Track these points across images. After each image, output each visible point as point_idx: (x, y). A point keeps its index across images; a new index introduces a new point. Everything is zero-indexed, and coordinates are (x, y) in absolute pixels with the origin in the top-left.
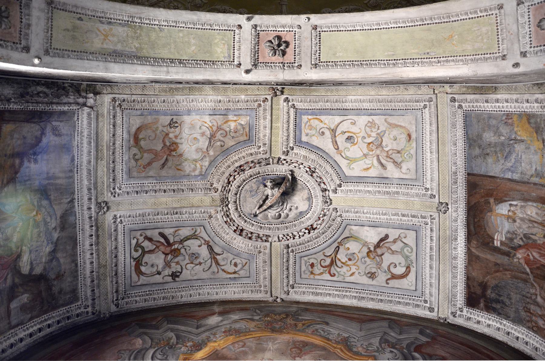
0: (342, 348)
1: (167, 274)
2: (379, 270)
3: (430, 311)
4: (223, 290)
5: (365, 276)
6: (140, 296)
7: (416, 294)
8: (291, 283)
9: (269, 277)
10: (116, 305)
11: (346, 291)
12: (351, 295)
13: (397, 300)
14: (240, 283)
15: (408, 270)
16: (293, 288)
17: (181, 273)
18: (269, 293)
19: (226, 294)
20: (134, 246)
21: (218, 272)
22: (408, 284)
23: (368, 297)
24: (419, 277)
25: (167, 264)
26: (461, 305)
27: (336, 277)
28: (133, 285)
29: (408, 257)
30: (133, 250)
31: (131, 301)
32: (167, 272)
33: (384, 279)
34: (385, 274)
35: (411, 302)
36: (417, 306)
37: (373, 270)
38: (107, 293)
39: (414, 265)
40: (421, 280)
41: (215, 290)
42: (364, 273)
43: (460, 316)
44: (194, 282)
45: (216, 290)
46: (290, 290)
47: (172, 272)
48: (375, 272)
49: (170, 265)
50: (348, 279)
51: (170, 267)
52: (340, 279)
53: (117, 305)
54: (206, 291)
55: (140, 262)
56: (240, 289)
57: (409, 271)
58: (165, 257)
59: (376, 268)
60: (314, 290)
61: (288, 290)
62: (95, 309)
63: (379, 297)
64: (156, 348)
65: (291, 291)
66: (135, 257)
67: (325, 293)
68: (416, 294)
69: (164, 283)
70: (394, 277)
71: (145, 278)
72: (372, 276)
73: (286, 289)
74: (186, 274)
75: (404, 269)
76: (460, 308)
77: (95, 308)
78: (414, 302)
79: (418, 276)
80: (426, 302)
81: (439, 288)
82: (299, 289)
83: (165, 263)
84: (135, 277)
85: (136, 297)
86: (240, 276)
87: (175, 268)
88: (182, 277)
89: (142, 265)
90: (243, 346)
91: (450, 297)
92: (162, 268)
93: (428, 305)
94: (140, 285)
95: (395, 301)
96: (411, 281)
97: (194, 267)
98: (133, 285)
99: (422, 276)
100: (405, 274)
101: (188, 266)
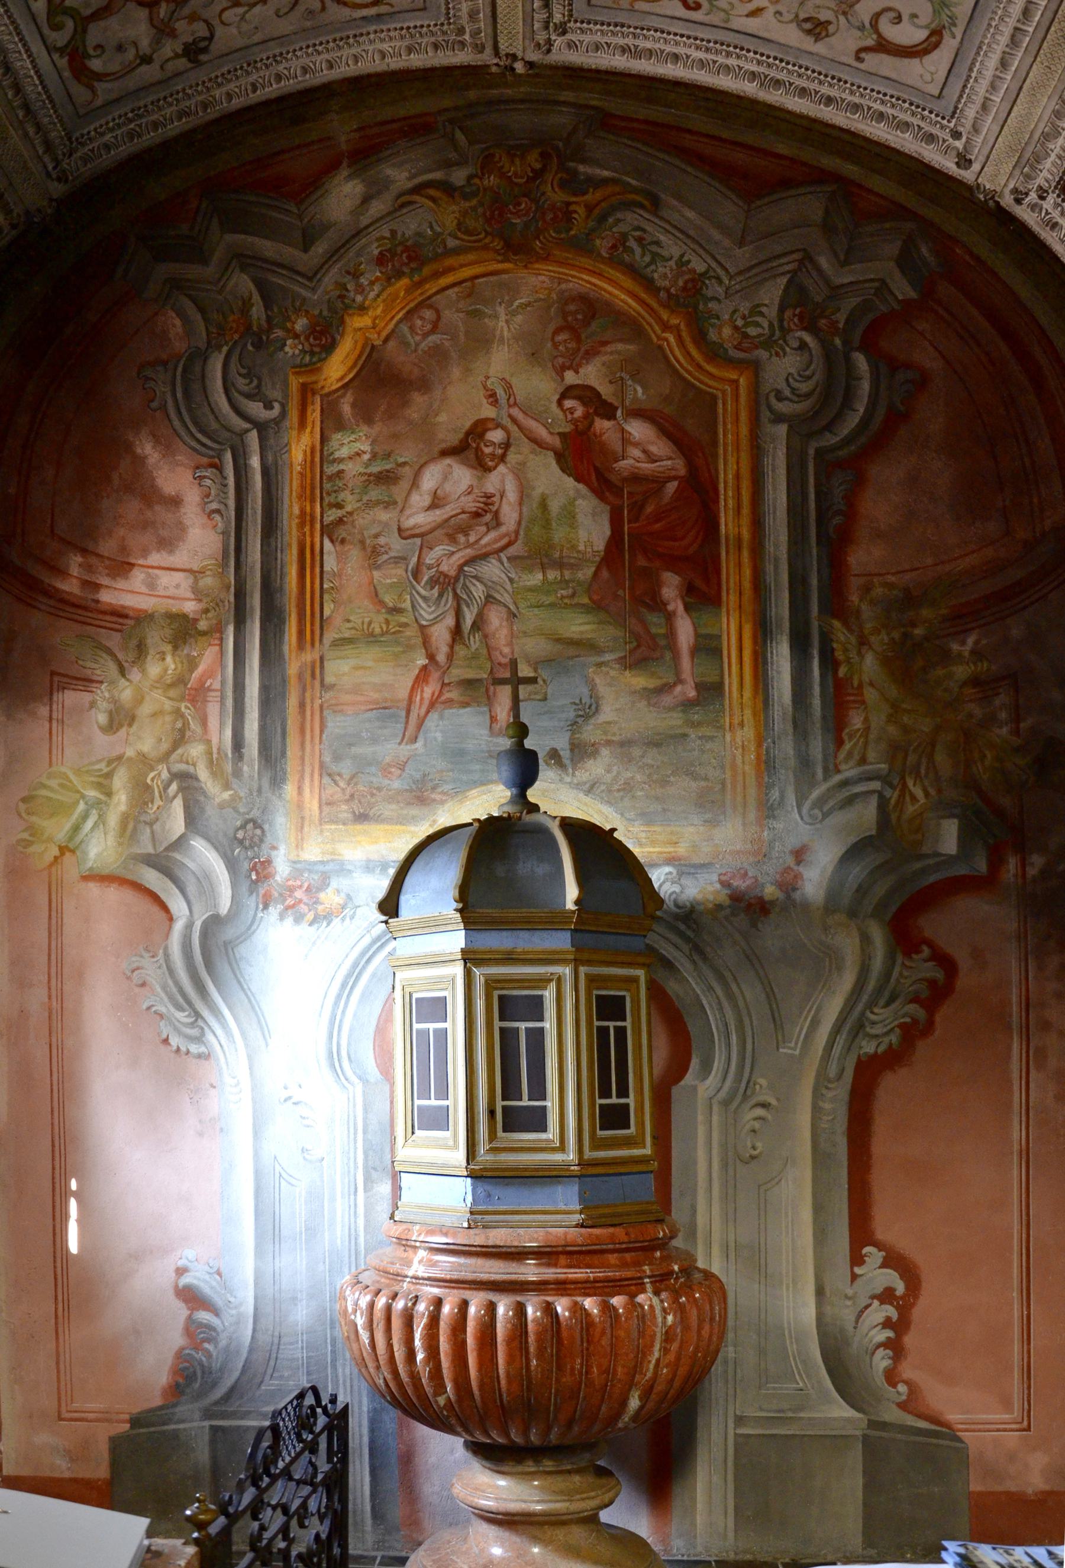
0: (683, 327)
1: (171, 54)
2: (842, 18)
3: (958, 164)
4: (346, 52)
5: (794, 25)
6: (112, 130)
7: (936, 106)
8: (557, 18)
9: (488, 10)
10: (59, 180)
11: (729, 54)
12: (740, 68)
13: (877, 106)
14: (399, 26)
15: (933, 39)
16: (564, 33)
17: (211, 38)
18: (489, 50)
19: (357, 62)
20: (45, 17)
21: (323, 8)
22: (921, 76)
23: (791, 84)
24: (962, 69)
25: (163, 30)
26: (1047, 181)
27: (700, 12)
28: (82, 111)
29: (947, 6)
30: (46, 31)
31: (92, 150)
32: (169, 48)
33: (853, 45)
34: (859, 34)
35: (915, 121)
36: (930, 138)
37: (824, 15)
38: (25, 162)
39: (958, 32)
40: (964, 78)
41: (322, 56)
42: (792, 17)
43: (1033, 207)
44: (255, 49)
45: (325, 56)
46: (553, 37)
47: (184, 44)
48: (829, 23)
49: (174, 30)
50: (738, 23)
51: (173, 34)
52: (716, 19)
53: (62, 179)
54: (296, 65)
55: (81, 50)
56: (398, 44)
57: (936, 45)
58: (150, 13)
59: (836, 12)
60: (630, 41)
61: (549, 39)
62: (15, 215)
63: (825, 90)
64: (225, 349)
65: (559, 41)
66: (59, 44)
67: (662, 52)
68: (936, 106)
69: (169, 78)
70: (884, 47)
71: (109, 86)
72: (818, 30)
73: (541, 37)
74: (227, 37)
75: (921, 35)
76: (1040, 188)
77: (11, 211)
78: (922, 124)
79: (957, 64)
80: (956, 135)
81: (1005, 121)
82: (582, 37)
83: (155, 31)
84: (80, 92)
85: (102, 134)
86: (396, 9)
87: (187, 31)
88: (216, 47)
89: (90, 57)
90: (434, 329)
91: (1027, 155)
92: (150, 45)
93: (959, 144)
94: (103, 106)
95: (869, 108)
96: (933, 69)
97: (246, 12)
98: (82, 111)
99: (971, 70)
100: (920, 48)
101: (228, 15)
